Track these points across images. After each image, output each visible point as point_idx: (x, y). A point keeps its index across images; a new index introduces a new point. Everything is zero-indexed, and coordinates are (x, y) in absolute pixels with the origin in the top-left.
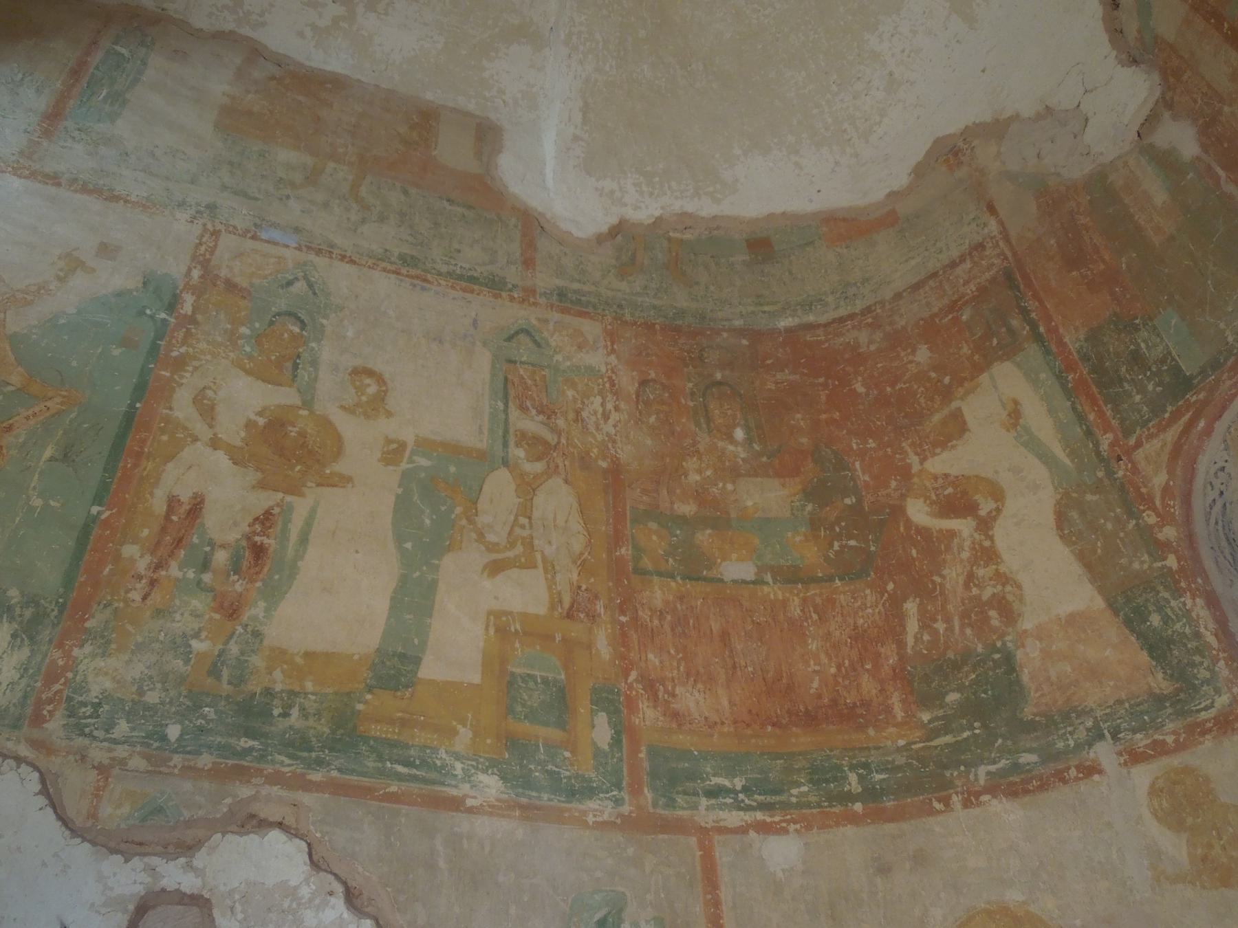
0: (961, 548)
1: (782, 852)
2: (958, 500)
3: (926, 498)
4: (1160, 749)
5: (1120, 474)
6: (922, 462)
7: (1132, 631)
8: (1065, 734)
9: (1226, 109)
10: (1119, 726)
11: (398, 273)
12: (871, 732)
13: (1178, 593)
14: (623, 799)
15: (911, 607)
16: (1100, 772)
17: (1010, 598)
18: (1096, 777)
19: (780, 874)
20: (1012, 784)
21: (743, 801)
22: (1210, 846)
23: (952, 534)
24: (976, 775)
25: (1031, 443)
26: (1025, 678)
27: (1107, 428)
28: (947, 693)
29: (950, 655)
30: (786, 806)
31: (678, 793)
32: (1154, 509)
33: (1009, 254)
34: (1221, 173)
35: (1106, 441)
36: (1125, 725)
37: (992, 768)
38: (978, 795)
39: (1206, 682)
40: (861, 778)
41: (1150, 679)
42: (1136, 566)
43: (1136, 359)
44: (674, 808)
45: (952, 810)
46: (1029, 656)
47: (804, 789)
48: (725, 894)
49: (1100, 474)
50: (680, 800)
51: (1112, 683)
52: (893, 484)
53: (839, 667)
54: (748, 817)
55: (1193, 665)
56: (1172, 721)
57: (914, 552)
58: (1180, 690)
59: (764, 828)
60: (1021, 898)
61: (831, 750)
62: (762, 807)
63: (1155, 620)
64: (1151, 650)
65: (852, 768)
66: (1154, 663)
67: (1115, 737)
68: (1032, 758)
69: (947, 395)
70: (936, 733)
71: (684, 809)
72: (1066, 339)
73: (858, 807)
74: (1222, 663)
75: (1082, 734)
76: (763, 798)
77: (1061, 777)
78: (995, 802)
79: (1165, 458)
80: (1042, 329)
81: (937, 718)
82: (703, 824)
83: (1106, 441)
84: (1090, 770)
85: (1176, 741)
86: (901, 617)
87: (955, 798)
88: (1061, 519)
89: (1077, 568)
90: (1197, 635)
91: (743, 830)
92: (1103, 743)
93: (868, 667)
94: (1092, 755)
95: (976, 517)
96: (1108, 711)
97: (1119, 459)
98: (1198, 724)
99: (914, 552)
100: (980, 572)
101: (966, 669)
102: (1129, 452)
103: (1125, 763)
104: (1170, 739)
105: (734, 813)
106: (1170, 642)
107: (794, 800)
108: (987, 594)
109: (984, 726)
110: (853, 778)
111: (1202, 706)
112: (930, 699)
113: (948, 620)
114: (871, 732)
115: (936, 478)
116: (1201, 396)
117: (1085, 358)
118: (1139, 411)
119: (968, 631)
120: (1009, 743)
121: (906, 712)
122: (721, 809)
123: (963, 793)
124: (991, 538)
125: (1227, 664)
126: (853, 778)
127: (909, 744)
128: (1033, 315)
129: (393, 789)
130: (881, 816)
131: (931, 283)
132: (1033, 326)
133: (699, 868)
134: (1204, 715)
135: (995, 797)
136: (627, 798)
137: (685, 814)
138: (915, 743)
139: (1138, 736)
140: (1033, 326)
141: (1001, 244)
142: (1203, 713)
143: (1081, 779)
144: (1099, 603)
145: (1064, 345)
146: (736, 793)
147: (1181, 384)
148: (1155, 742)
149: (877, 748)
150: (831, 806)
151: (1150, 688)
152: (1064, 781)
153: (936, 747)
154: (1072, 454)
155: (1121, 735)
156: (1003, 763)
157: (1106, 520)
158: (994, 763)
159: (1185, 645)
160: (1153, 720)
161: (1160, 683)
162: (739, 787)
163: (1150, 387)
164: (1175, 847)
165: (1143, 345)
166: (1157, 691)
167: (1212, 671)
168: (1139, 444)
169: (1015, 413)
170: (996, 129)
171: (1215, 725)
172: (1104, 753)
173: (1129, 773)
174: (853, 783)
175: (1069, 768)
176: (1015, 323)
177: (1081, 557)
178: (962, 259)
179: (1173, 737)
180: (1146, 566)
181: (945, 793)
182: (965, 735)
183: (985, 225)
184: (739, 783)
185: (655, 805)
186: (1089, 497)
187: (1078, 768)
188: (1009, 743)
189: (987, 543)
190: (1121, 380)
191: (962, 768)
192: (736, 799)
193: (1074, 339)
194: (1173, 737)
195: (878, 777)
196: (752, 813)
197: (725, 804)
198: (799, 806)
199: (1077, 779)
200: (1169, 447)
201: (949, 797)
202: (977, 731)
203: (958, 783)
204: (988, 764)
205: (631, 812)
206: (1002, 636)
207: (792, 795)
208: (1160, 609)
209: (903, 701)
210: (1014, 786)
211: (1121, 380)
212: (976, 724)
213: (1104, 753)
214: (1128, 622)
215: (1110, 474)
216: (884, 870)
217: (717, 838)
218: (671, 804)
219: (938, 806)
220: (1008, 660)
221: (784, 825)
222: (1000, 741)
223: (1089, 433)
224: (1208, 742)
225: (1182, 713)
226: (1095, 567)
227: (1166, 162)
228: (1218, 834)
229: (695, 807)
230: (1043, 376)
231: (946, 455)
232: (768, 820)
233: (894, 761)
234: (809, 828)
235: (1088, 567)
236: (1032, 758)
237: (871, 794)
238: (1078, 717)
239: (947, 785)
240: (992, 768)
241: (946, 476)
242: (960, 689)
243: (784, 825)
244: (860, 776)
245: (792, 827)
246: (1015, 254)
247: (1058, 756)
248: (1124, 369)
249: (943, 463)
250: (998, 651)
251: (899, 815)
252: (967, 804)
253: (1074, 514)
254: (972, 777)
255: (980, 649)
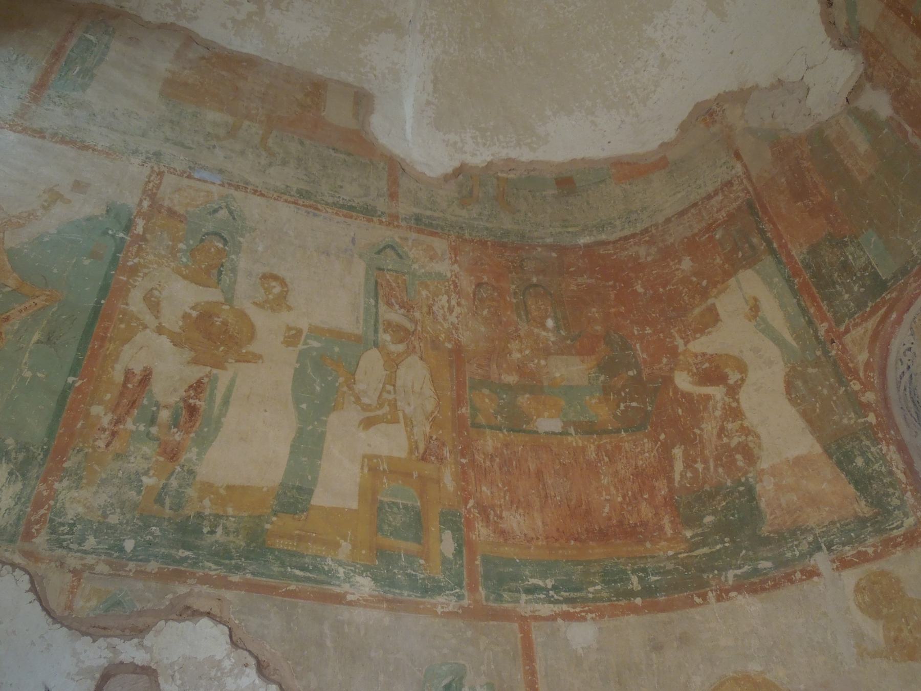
0: (715, 408)
1: (582, 634)
2: (712, 372)
3: (689, 371)
4: (863, 558)
5: (834, 353)
6: (686, 344)
7: (843, 470)
8: (792, 546)
9: (912, 81)
10: (832, 541)
11: (296, 203)
12: (648, 545)
13: (876, 441)
14: (463, 595)
15: (678, 452)
16: (819, 575)
17: (751, 445)
18: (816, 579)
19: (580, 651)
20: (753, 584)
21: (553, 596)
22: (900, 630)
23: (708, 398)
24: (726, 577)
25: (767, 330)
26: (763, 505)
27: (824, 319)
28: (704, 516)
29: (707, 488)
30: (585, 600)
31: (504, 590)
32: (859, 379)
33: (751, 189)
34: (909, 129)
35: (823, 328)
36: (837, 540)
37: (738, 572)
38: (727, 592)
39: (897, 508)
40: (641, 580)
41: (856, 505)
42: (845, 421)
43: (845, 267)
44: (502, 601)
45: (708, 603)
46: (766, 489)
47: (598, 587)
48: (539, 666)
49: (819, 353)
50: (506, 595)
51: (827, 509)
52: (665, 360)
53: (624, 497)
54: (557, 608)
55: (887, 495)
56: (872, 537)
57: (680, 411)
58: (878, 514)
59: (568, 617)
60: (759, 669)
61: (618, 559)
62: (567, 601)
63: (859, 462)
64: (856, 484)
65: (634, 572)
66: (859, 494)
67: (829, 548)
68: (768, 564)
69: (704, 294)
70: (696, 546)
71: (509, 602)
72: (793, 253)
73: (638, 601)
74: (909, 493)
75: (805, 547)
76: (567, 594)
77: (789, 579)
78: (740, 597)
79: (867, 341)
80: (775, 245)
81: (697, 535)
82: (523, 614)
83: (823, 328)
84: (811, 574)
85: (875, 552)
86: (671, 460)
87: (710, 594)
88: (789, 386)
89: (801, 423)
90: (891, 473)
91: (552, 618)
92: (820, 553)
93: (646, 496)
94: (812, 562)
95: (726, 385)
96: (824, 529)
97: (833, 342)
98: (891, 539)
99: (680, 411)
100: (729, 426)
101: (719, 498)
102: (840, 336)
103: (837, 568)
104: (870, 550)
105: (546, 605)
106: (870, 478)
107: (591, 596)
108: (734, 442)
109: (732, 541)
110: (635, 579)
111: (894, 526)
112: (692, 521)
113: (705, 462)
114: (648, 545)
115: (696, 356)
116: (894, 295)
117: (807, 266)
118: (848, 306)
119: (720, 470)
120: (751, 553)
121: (674, 530)
122: (536, 603)
123: (716, 591)
124: (737, 401)
125: (912, 494)
126: (635, 579)
127: (677, 554)
128: (769, 235)
129: (293, 587)
130: (655, 608)
131: (693, 211)
132: (769, 242)
133: (520, 647)
134: (895, 533)
135: (740, 593)
136: (466, 594)
137: (510, 606)
138: (681, 553)
139: (847, 548)
140: (769, 242)
141: (745, 181)
142: (895, 531)
143: (804, 580)
144: (818, 449)
145: (792, 257)
146: (548, 590)
147: (878, 286)
148: (859, 552)
149: (653, 557)
150: (618, 600)
151: (856, 512)
152: (792, 582)
153: (696, 556)
154: (798, 338)
155: (834, 548)
156: (746, 568)
157: (823, 387)
158: (740, 568)
159: (882, 480)
160: (858, 536)
161: (863, 508)
162: (550, 586)
163: (856, 288)
164: (874, 631)
165: (850, 257)
166: (861, 515)
167: (902, 500)
168: (847, 331)
169: (755, 308)
170: (741, 96)
171: (904, 540)
172: (821, 560)
173: (840, 575)
174: (635, 583)
175: (795, 572)
176: (755, 240)
177: (804, 415)
178: (716, 193)
179: (873, 549)
180: (852, 422)
181: (703, 591)
182: (718, 547)
183: (733, 167)
184: (549, 583)
185: (487, 599)
186: (810, 370)
187: (802, 572)
188: (751, 553)
189: (734, 405)
190: (834, 283)
191: (716, 572)
192: (547, 595)
193: (799, 252)
194: (873, 549)
195: (653, 578)
196: (560, 606)
197: (540, 599)
198: (595, 600)
199: (801, 580)
200: (870, 333)
201: (706, 594)
202: (727, 545)
203: (713, 583)
204: (735, 569)
205: (470, 605)
206: (745, 474)
207: (589, 592)
208: (863, 454)
209: (672, 522)
210: (754, 585)
211: (834, 283)
212: (726, 539)
213: (821, 560)
214: (839, 463)
215: (826, 353)
216: (658, 648)
217: (533, 624)
218: (499, 598)
219: (698, 600)
220: (750, 492)
221: (583, 614)
222: (744, 552)
223: (810, 323)
224: (899, 553)
225: (879, 531)
226: (815, 422)
227: (868, 121)
228: (906, 621)
229: (517, 601)
230: (776, 280)
231: (703, 339)
232: (572, 610)
233: (665, 566)
234: (602, 616)
235: (810, 422)
236: (768, 564)
237: (648, 591)
238: (802, 534)
239: (705, 584)
240: (738, 572)
241: (704, 354)
242: (714, 513)
243: (583, 614)
244: (640, 578)
245: (589, 616)
246: (755, 189)
247: (787, 563)
248: (836, 275)
249: (701, 345)
250: (743, 485)
251: (669, 607)
252: (719, 599)
253: (799, 383)
254: (723, 579)
255: (729, 483)
